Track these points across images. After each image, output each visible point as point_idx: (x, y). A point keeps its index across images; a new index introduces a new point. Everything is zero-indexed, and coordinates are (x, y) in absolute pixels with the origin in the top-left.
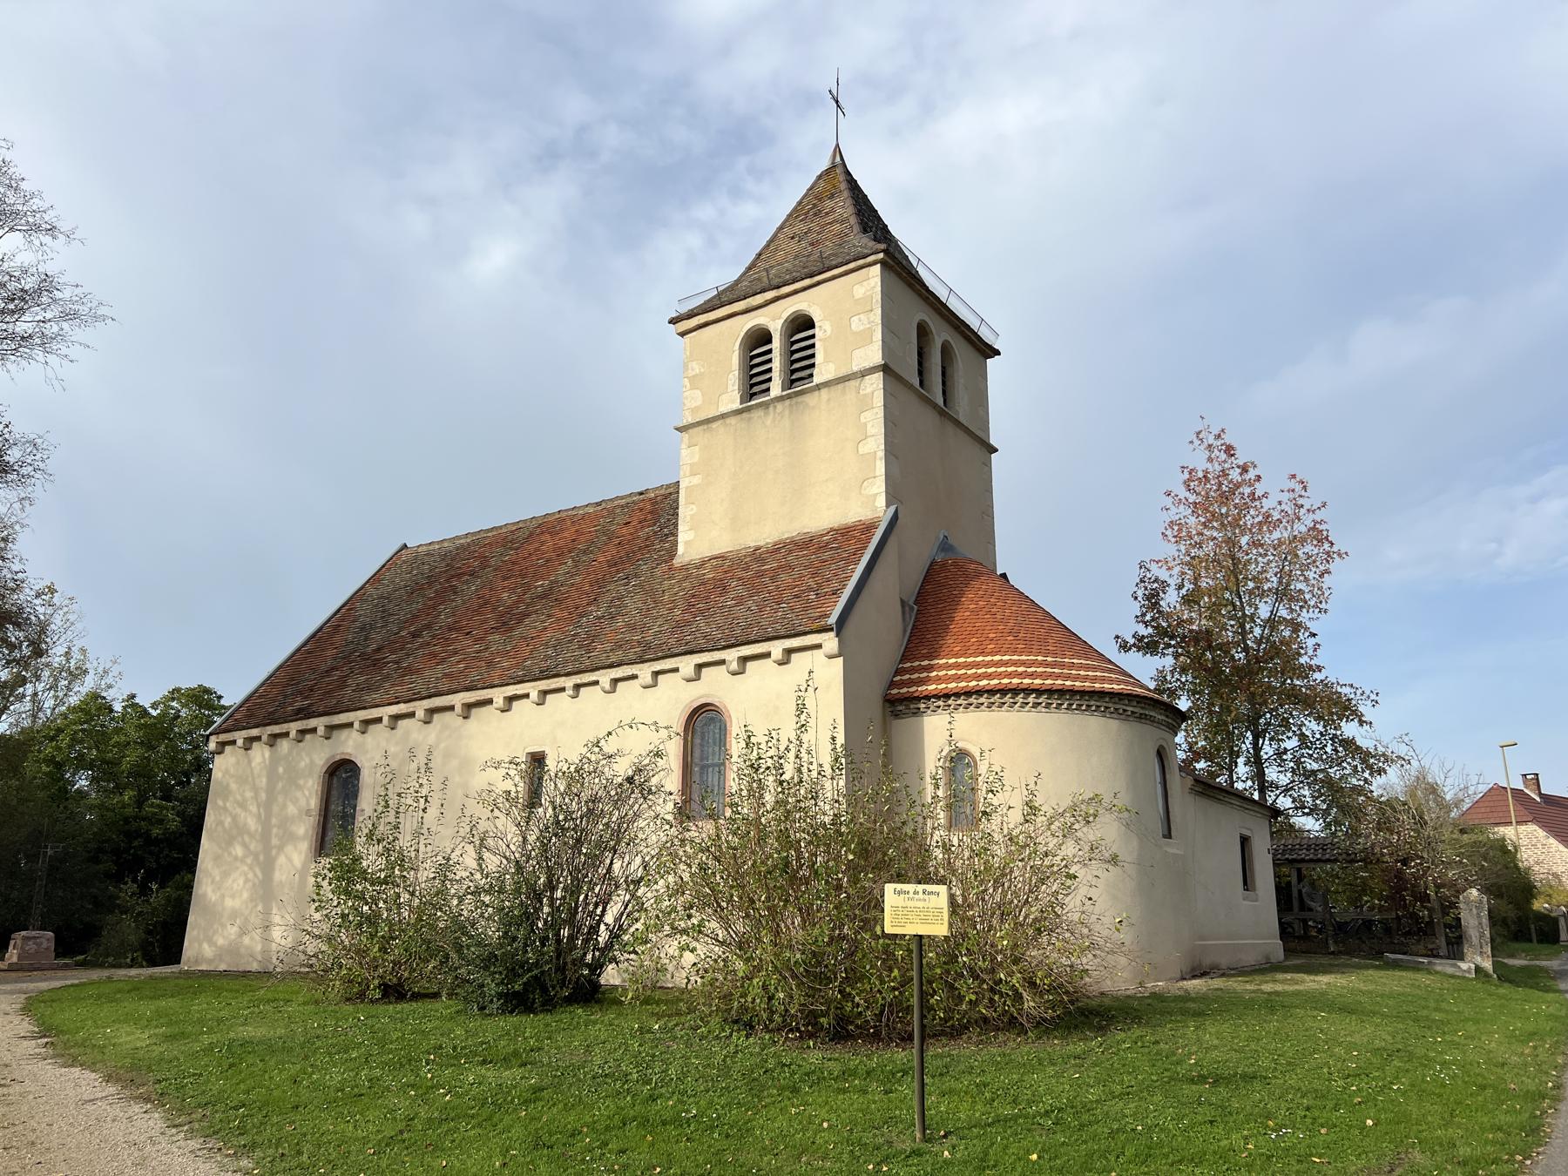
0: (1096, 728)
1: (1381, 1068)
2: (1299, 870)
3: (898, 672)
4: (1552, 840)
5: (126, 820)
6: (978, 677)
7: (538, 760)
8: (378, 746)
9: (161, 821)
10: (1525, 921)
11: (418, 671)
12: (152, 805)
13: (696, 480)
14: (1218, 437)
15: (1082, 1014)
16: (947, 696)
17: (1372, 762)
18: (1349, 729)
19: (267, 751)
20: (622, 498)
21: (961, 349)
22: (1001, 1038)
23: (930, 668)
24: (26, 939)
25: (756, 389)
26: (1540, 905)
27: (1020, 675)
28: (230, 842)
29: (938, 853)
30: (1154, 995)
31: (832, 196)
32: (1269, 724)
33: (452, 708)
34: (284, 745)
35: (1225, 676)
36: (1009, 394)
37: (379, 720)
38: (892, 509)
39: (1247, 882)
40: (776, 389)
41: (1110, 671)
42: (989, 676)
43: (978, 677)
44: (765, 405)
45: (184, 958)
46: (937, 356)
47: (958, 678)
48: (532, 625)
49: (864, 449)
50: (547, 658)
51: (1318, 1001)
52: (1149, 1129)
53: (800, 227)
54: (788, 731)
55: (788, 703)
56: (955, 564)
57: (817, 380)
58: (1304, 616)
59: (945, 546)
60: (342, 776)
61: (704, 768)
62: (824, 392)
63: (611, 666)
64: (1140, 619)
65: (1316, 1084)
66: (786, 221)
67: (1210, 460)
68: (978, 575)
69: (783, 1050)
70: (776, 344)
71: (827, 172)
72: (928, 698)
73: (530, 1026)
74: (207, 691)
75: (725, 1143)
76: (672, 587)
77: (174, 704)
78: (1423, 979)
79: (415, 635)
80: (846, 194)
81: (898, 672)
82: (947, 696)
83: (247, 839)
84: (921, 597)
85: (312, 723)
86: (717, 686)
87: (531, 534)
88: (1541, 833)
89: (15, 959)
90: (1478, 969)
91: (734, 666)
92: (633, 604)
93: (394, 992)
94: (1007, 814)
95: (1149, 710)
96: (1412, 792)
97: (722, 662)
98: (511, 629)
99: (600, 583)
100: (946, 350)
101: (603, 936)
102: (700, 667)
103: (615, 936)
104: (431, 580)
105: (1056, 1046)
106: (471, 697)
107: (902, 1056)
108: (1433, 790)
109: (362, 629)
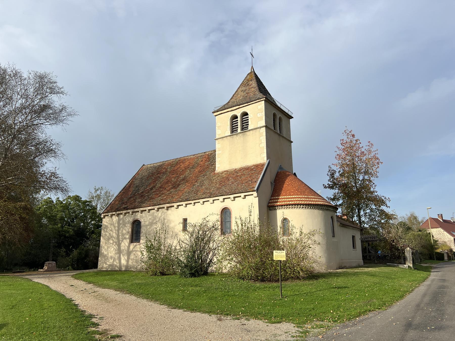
0: (317, 212)
1: (374, 286)
2: (369, 243)
3: (270, 200)
4: (445, 232)
5: (59, 232)
6: (289, 201)
7: (185, 220)
8: (145, 217)
9: (68, 232)
10: (430, 256)
11: (154, 198)
12: (66, 228)
13: (220, 152)
14: (350, 132)
15: (312, 276)
16: (282, 206)
17: (389, 217)
18: (383, 208)
19: (117, 218)
20: (200, 154)
21: (284, 118)
22: (296, 281)
23: (278, 199)
24: (48, 263)
25: (234, 130)
26: (439, 251)
27: (299, 201)
28: (109, 239)
29: (281, 243)
30: (330, 273)
31: (251, 80)
32: (362, 206)
33: (164, 208)
34: (122, 216)
35: (353, 192)
36: (296, 127)
37: (146, 210)
38: (268, 160)
39: (354, 246)
40: (239, 130)
41: (320, 199)
42: (292, 201)
43: (289, 201)
44: (237, 134)
45: (99, 267)
46: (278, 121)
47: (284, 201)
48: (181, 187)
49: (261, 146)
50: (186, 196)
51: (367, 274)
52: (324, 296)
53: (244, 88)
54: (247, 215)
55: (245, 208)
56: (283, 173)
57: (249, 128)
58: (372, 179)
59: (281, 168)
60: (136, 225)
61: (225, 222)
62: (251, 131)
63: (203, 198)
64: (329, 180)
65: (359, 289)
66: (240, 86)
67: (348, 138)
68: (289, 175)
69: (251, 283)
70: (239, 119)
71: (250, 73)
72: (278, 206)
73: (197, 280)
74: (78, 196)
75: (245, 299)
76: (215, 179)
77: (69, 200)
78: (394, 269)
79: (151, 189)
80: (255, 80)
81: (270, 200)
82: (282, 206)
83: (113, 239)
84: (275, 181)
85: (129, 211)
86: (228, 203)
87: (177, 163)
88: (442, 230)
89: (46, 268)
90: (409, 266)
91: (232, 199)
92: (206, 183)
93: (163, 274)
94: (296, 234)
95: (327, 208)
96: (409, 219)
97: (230, 198)
98: (176, 188)
99: (197, 177)
100: (280, 119)
101: (208, 260)
102: (224, 199)
103: (211, 261)
104: (153, 174)
105: (307, 282)
106: (168, 205)
107: (275, 284)
108: (415, 218)
109: (137, 187)
